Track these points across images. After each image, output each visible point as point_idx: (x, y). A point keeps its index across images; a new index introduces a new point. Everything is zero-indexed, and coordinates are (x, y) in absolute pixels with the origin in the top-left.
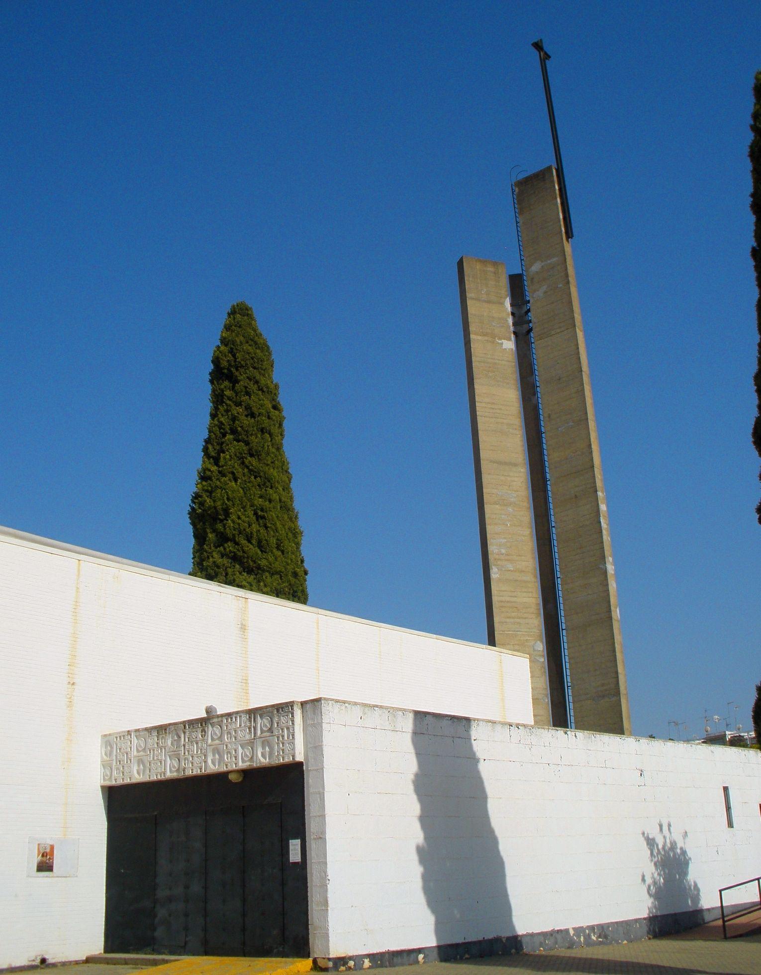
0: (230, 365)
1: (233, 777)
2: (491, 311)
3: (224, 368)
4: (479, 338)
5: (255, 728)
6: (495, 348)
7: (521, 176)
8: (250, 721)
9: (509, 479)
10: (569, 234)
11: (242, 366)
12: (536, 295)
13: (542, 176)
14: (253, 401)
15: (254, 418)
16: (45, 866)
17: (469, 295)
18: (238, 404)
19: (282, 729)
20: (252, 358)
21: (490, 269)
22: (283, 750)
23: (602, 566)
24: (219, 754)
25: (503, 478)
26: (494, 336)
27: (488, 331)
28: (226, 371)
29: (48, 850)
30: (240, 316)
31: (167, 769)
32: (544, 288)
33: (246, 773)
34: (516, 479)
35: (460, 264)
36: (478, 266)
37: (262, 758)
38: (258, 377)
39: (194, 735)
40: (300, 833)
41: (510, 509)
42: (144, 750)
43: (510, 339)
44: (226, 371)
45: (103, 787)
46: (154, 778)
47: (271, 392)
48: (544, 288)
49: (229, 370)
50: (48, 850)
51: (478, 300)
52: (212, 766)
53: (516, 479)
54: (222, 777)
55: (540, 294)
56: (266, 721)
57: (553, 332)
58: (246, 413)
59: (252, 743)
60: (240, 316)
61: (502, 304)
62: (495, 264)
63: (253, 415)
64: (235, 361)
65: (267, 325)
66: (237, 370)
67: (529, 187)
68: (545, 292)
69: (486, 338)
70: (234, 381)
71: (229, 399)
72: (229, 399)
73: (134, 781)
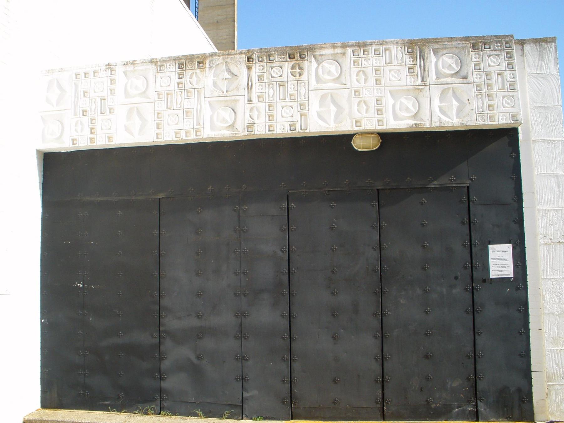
1: (358, 144)
8: (414, 58)
33: (388, 139)
39: (276, 72)
46: (168, 137)
54: (336, 145)
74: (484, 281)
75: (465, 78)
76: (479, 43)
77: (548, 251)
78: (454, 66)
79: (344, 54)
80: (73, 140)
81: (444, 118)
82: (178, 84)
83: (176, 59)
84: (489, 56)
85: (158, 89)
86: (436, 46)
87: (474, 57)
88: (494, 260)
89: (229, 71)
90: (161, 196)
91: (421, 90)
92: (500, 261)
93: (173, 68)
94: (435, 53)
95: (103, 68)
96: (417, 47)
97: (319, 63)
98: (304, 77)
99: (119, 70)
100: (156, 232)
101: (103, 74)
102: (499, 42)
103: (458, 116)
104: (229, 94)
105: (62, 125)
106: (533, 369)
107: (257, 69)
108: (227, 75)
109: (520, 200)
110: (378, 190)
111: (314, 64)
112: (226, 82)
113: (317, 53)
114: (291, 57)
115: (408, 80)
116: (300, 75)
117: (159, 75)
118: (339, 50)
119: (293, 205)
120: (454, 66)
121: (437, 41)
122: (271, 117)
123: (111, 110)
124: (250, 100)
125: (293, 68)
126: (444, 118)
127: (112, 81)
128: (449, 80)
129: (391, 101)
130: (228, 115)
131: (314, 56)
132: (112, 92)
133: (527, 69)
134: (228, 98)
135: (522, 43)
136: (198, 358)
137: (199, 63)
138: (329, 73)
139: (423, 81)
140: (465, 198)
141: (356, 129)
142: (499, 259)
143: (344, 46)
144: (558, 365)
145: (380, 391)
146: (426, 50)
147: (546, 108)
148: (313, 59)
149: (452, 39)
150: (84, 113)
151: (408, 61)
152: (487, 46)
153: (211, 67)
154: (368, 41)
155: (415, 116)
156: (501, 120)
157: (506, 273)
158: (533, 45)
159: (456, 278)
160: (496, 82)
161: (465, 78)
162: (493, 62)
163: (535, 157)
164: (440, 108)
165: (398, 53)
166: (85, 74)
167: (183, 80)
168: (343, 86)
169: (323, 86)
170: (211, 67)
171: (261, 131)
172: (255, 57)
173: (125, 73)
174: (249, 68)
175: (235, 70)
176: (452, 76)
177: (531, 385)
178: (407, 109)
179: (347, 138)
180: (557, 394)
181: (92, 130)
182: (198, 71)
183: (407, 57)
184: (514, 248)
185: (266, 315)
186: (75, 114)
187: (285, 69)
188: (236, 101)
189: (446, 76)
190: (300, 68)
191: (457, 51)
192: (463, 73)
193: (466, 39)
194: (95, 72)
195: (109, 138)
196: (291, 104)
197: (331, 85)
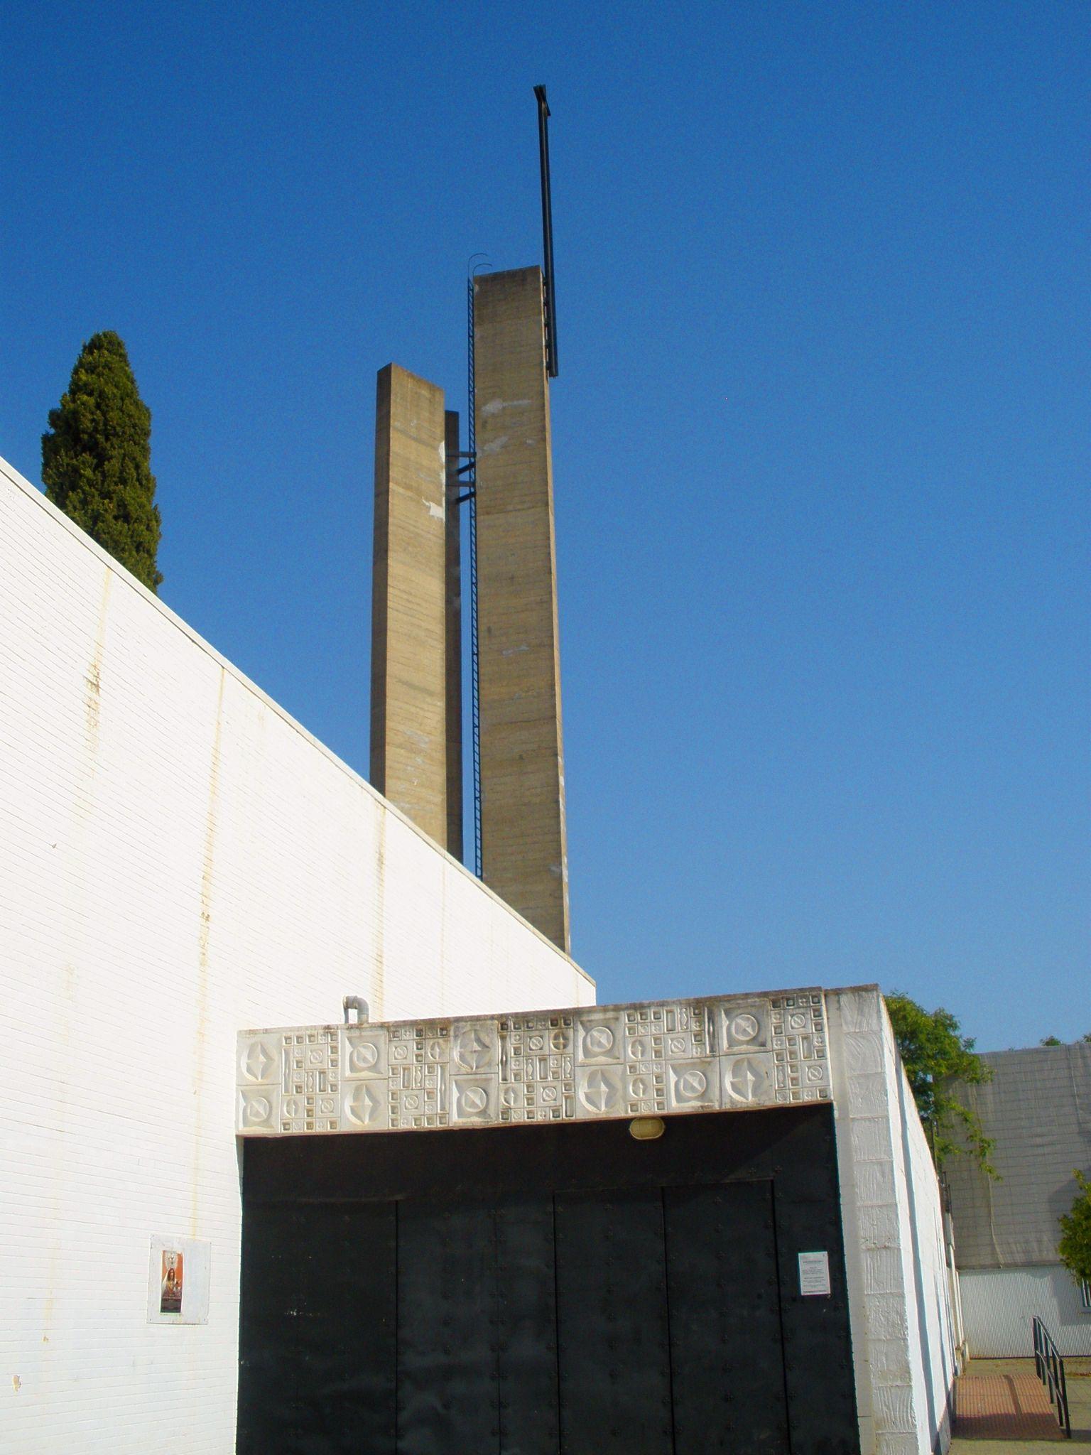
0: (96, 430)
1: (636, 1131)
2: (419, 457)
3: (84, 432)
4: (401, 490)
5: (713, 1036)
6: (419, 513)
7: (482, 271)
8: (701, 1022)
9: (421, 713)
10: (552, 369)
11: (116, 435)
12: (491, 450)
13: (520, 277)
14: (128, 493)
15: (129, 523)
16: (171, 1303)
17: (395, 423)
18: (107, 495)
19: (791, 1040)
20: (134, 426)
21: (425, 393)
22: (794, 1081)
23: (554, 868)
24: (608, 1084)
25: (413, 709)
26: (419, 492)
27: (414, 484)
28: (86, 437)
29: (175, 1266)
30: (102, 354)
31: (460, 1109)
32: (504, 439)
33: (672, 1123)
34: (429, 715)
35: (384, 377)
36: (410, 384)
37: (735, 1092)
38: (139, 458)
39: (534, 1044)
40: (830, 1238)
41: (419, 760)
42: (374, 1068)
43: (440, 505)
44: (86, 437)
45: (237, 1137)
46: (406, 1123)
47: (145, 483)
48: (504, 439)
49: (91, 436)
50: (175, 1266)
51: (404, 432)
52: (674, 1103)
53: (429, 715)
54: (612, 1132)
55: (495, 446)
56: (744, 1024)
57: (510, 508)
58: (115, 513)
59: (704, 1065)
60: (102, 354)
61: (436, 449)
62: (432, 388)
63: (126, 518)
64: (105, 424)
65: (153, 380)
66: (107, 439)
67: (494, 291)
68: (503, 447)
69: (409, 494)
70: (101, 458)
71: (91, 483)
72: (91, 483)
73: (343, 1128)
74: (794, 1299)
75: (763, 1045)
76: (780, 1000)
77: (872, 1259)
78: (749, 1030)
79: (617, 1019)
80: (285, 1124)
81: (735, 1096)
82: (417, 1056)
83: (413, 1024)
84: (792, 1016)
85: (393, 1061)
86: (728, 1005)
87: (774, 1019)
88: (805, 1272)
89: (478, 1040)
90: (399, 1197)
91: (709, 1063)
92: (813, 1273)
93: (410, 1036)
94: (727, 1014)
95: (321, 1032)
96: (705, 1008)
97: (587, 1030)
98: (570, 1049)
99: (341, 1035)
100: (393, 1244)
101: (321, 1039)
102: (805, 997)
103: (754, 1095)
104: (481, 1070)
105: (271, 1107)
106: (859, 1413)
107: (512, 1042)
108: (476, 1047)
109: (837, 1195)
110: (662, 1188)
111: (581, 1033)
112: (475, 1056)
113: (585, 1018)
114: (554, 1023)
115: (694, 1052)
116: (565, 1046)
117: (394, 1044)
118: (610, 1015)
119: (560, 1209)
120: (749, 1030)
121: (729, 998)
122: (530, 1101)
123: (334, 1088)
124: (504, 1079)
125: (556, 1037)
126: (735, 1096)
127: (334, 1050)
128: (744, 1048)
129: (673, 1078)
130: (477, 1098)
131: (582, 1023)
132: (334, 1063)
133: (844, 1027)
134: (478, 1077)
135: (838, 992)
136: (446, 1406)
137: (442, 1029)
138: (600, 1044)
139: (712, 1050)
140: (768, 1196)
141: (631, 1114)
142: (813, 1271)
143: (617, 1009)
144: (888, 1407)
145: (670, 1446)
146: (716, 1010)
147: (866, 1076)
148: (580, 1027)
149: (747, 996)
150: (299, 1089)
151: (694, 1027)
152: (791, 1002)
153: (456, 1036)
154: (646, 1002)
155: (703, 1096)
156: (808, 1097)
157: (822, 1288)
158: (850, 995)
159: (760, 1296)
160: (800, 1047)
161: (763, 1045)
162: (797, 1023)
163: (855, 1140)
164: (732, 1084)
165: (682, 1016)
166: (298, 1038)
167: (422, 1052)
168: (615, 1061)
169: (593, 1060)
170: (456, 1036)
171: (519, 1117)
172: (511, 1024)
173: (350, 1039)
174: (503, 1038)
175: (486, 1040)
176: (748, 1043)
177: (857, 1436)
178: (693, 1088)
179: (624, 1123)
180: (888, 1446)
181: (310, 1113)
182: (441, 1041)
183: (693, 1020)
184: (830, 1256)
185: (529, 1348)
186: (287, 1091)
187: (546, 1039)
188: (488, 1080)
189: (742, 1043)
190: (565, 1038)
191: (754, 1010)
192: (760, 1039)
193: (764, 994)
194: (310, 1036)
195: (332, 1123)
196: (555, 1084)
197: (602, 1059)
